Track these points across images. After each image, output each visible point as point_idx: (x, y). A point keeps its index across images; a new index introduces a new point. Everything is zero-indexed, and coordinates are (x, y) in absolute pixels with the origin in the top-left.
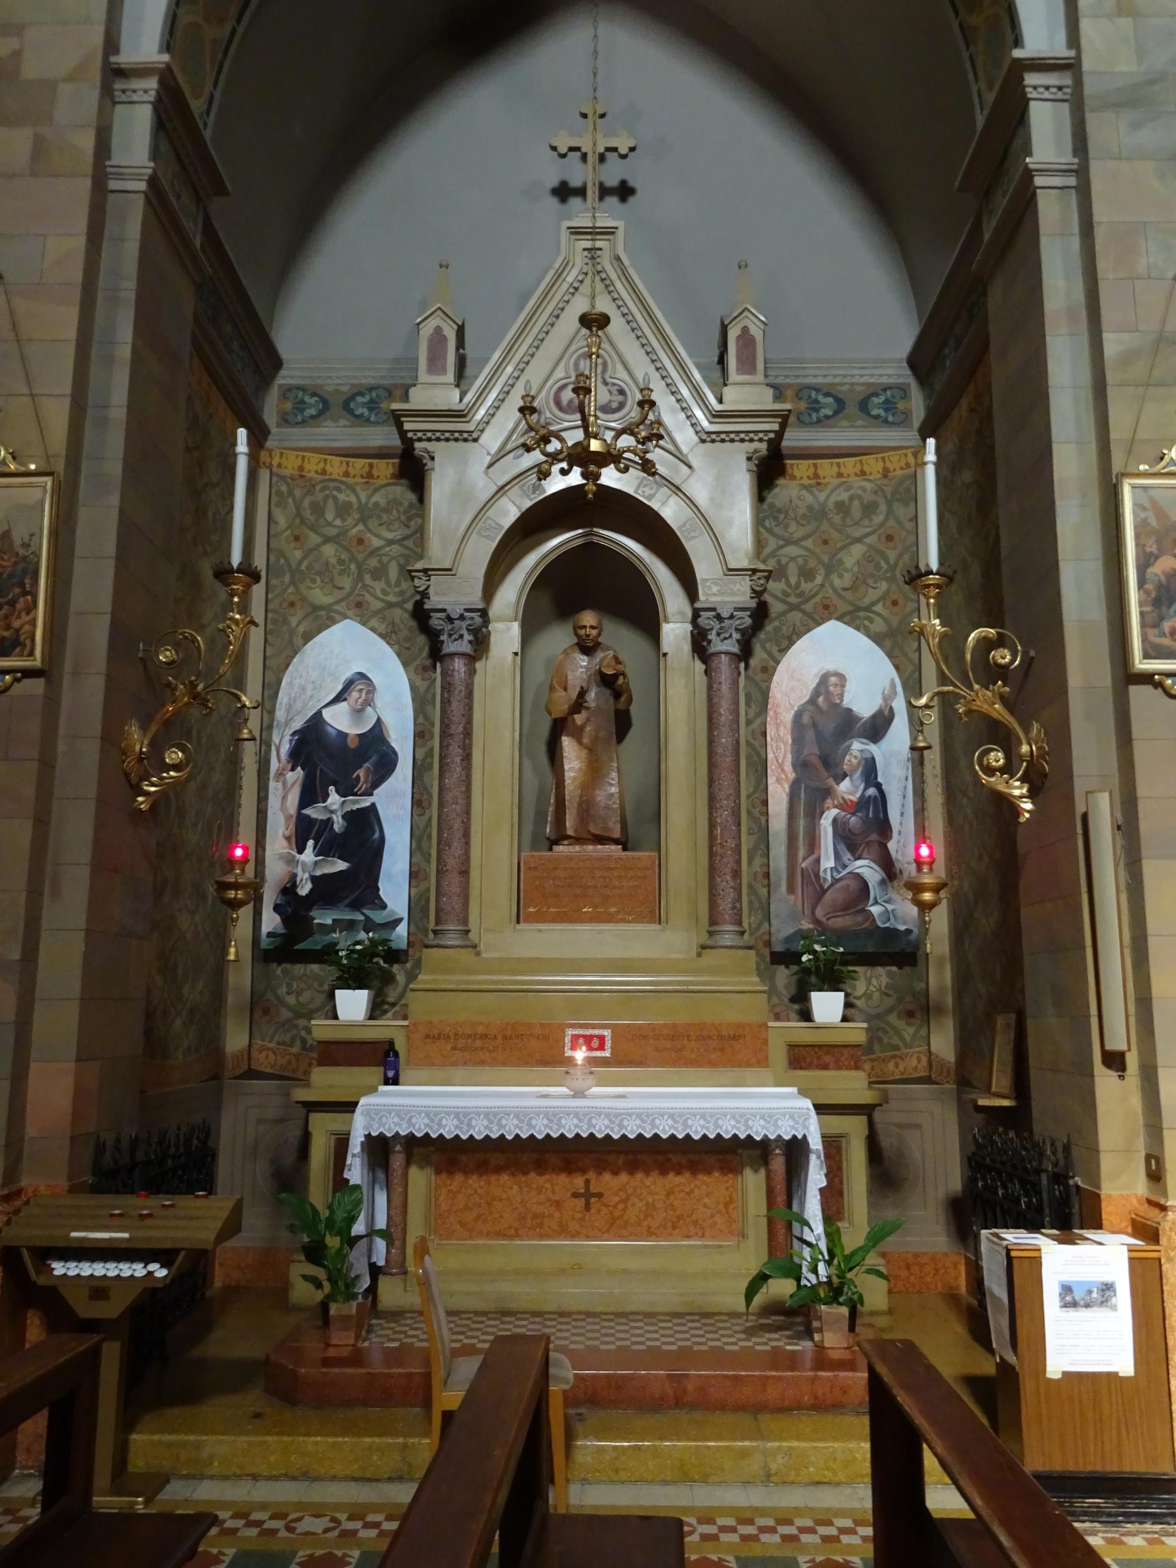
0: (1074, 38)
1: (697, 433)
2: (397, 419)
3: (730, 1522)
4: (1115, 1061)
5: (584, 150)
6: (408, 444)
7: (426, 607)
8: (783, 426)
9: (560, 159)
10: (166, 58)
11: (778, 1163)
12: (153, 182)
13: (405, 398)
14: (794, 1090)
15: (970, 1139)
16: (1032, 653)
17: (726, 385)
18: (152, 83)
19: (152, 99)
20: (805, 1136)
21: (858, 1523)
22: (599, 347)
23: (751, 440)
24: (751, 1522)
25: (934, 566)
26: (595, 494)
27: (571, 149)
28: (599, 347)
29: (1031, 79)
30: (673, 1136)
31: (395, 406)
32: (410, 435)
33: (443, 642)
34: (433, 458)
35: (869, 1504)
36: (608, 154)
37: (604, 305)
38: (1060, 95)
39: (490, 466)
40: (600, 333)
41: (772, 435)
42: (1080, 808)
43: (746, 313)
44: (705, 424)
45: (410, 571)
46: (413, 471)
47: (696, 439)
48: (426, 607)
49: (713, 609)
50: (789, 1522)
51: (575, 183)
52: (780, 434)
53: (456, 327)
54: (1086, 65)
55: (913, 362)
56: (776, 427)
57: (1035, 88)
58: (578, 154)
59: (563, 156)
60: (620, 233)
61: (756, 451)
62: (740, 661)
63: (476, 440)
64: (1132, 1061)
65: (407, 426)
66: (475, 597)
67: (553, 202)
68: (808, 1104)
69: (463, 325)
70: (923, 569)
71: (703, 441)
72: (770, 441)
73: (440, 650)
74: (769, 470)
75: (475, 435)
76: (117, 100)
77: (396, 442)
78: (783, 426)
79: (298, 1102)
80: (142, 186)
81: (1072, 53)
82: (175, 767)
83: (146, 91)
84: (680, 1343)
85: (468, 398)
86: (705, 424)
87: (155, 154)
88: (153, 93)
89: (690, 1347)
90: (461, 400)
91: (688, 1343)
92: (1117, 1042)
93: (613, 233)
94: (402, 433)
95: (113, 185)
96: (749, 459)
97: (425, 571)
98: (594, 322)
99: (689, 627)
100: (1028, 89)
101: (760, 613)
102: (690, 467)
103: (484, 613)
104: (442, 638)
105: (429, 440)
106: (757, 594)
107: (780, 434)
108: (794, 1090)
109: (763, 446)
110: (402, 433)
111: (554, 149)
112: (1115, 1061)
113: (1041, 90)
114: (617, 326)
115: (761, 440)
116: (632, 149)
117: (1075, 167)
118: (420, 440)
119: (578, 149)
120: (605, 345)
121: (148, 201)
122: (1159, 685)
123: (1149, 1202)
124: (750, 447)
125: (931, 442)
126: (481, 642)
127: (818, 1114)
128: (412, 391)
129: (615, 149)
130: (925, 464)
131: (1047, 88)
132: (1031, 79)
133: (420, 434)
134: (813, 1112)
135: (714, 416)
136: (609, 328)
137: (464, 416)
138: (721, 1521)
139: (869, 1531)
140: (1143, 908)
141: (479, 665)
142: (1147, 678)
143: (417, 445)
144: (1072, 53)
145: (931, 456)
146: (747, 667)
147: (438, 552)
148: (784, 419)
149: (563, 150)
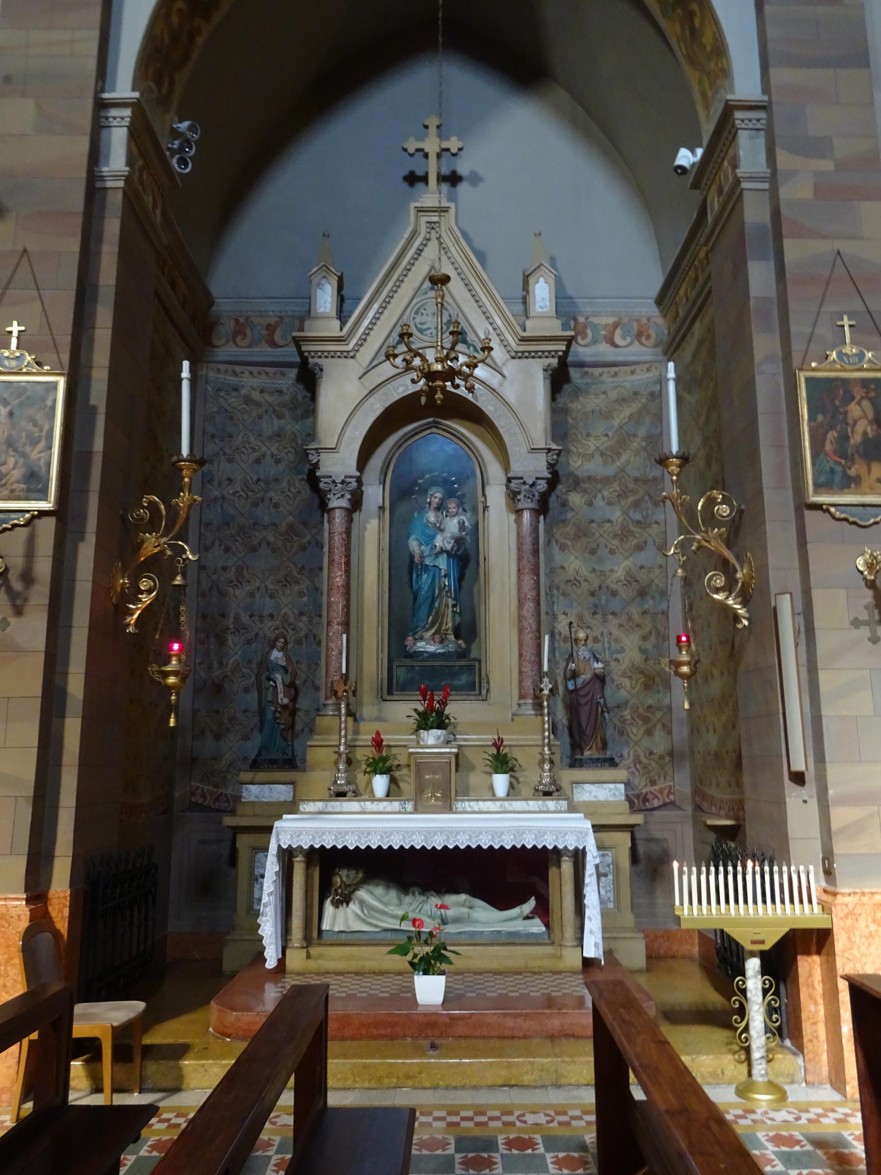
0: (766, 88)
1: (509, 352)
2: (297, 342)
3: (497, 1113)
4: (798, 778)
5: (426, 151)
6: (304, 361)
7: (317, 474)
8: (568, 347)
9: (411, 158)
10: (136, 95)
11: (567, 866)
12: (128, 180)
13: (302, 329)
14: (582, 815)
15: (809, 1056)
16: (743, 507)
17: (528, 318)
18: (127, 112)
19: (127, 124)
20: (584, 848)
21: (585, 1113)
22: (443, 299)
23: (546, 357)
24: (457, 1114)
25: (675, 449)
26: (442, 401)
27: (418, 150)
28: (443, 299)
29: (738, 115)
30: (491, 847)
31: (295, 334)
32: (306, 354)
33: (329, 499)
34: (321, 370)
35: (593, 1100)
36: (444, 153)
37: (447, 269)
38: (758, 126)
39: (360, 378)
40: (444, 288)
41: (561, 354)
42: (773, 604)
43: (542, 267)
44: (514, 345)
45: (306, 450)
46: (309, 378)
47: (508, 356)
48: (317, 474)
49: (522, 478)
50: (483, 1113)
51: (420, 172)
52: (566, 353)
53: (336, 278)
54: (775, 108)
55: (660, 301)
56: (563, 348)
57: (743, 121)
58: (421, 153)
59: (411, 155)
60: (452, 211)
61: (549, 365)
62: (539, 515)
63: (352, 357)
64: (810, 777)
65: (304, 348)
66: (353, 471)
67: (405, 185)
68: (588, 825)
69: (342, 275)
70: (668, 453)
71: (513, 358)
72: (560, 358)
73: (327, 505)
74: (559, 379)
75: (352, 354)
76: (102, 124)
77: (298, 359)
78: (568, 347)
79: (228, 827)
80: (121, 184)
81: (766, 98)
82: (149, 591)
83: (122, 118)
84: (499, 991)
85: (346, 329)
86: (514, 345)
87: (130, 162)
88: (128, 119)
89: (506, 995)
90: (341, 330)
91: (505, 992)
92: (798, 765)
93: (447, 211)
94: (301, 353)
95: (98, 185)
96: (544, 370)
97: (316, 449)
98: (439, 281)
99: (504, 488)
100: (737, 122)
101: (554, 480)
102: (504, 376)
103: (359, 480)
104: (329, 496)
105: (320, 357)
106: (551, 466)
107: (566, 353)
108: (582, 815)
109: (554, 362)
110: (301, 353)
111: (405, 150)
112: (798, 778)
113: (746, 122)
114: (455, 285)
115: (553, 357)
116: (460, 149)
117: (768, 175)
118: (313, 357)
119: (422, 150)
120: (447, 298)
121: (125, 193)
122: (828, 511)
123: (825, 891)
124: (546, 361)
125: (671, 365)
126: (356, 502)
127: (594, 832)
128: (307, 323)
129: (448, 150)
130: (668, 380)
131: (758, 120)
132: (738, 115)
133: (312, 354)
134: (591, 831)
135: (520, 340)
136: (450, 285)
137: (344, 341)
138: (490, 1114)
139: (593, 1118)
140: (812, 607)
141: (355, 516)
142: (818, 507)
143: (310, 360)
144: (766, 98)
145: (671, 374)
146: (545, 518)
147: (327, 438)
148: (570, 341)
149: (411, 150)
